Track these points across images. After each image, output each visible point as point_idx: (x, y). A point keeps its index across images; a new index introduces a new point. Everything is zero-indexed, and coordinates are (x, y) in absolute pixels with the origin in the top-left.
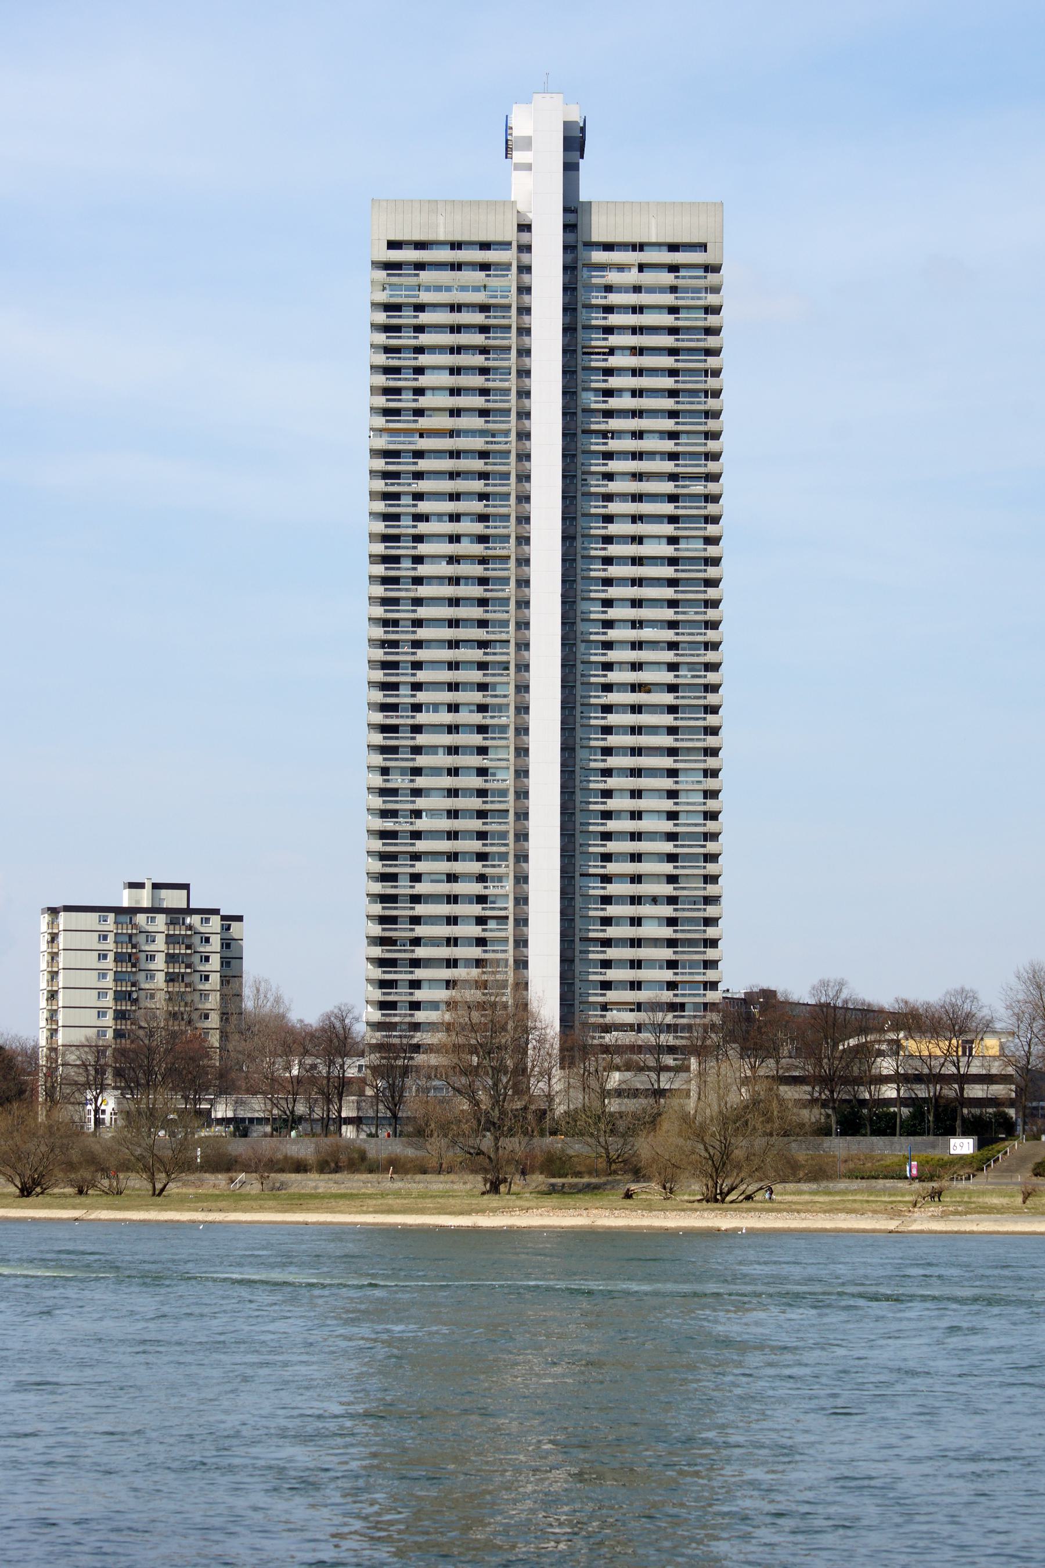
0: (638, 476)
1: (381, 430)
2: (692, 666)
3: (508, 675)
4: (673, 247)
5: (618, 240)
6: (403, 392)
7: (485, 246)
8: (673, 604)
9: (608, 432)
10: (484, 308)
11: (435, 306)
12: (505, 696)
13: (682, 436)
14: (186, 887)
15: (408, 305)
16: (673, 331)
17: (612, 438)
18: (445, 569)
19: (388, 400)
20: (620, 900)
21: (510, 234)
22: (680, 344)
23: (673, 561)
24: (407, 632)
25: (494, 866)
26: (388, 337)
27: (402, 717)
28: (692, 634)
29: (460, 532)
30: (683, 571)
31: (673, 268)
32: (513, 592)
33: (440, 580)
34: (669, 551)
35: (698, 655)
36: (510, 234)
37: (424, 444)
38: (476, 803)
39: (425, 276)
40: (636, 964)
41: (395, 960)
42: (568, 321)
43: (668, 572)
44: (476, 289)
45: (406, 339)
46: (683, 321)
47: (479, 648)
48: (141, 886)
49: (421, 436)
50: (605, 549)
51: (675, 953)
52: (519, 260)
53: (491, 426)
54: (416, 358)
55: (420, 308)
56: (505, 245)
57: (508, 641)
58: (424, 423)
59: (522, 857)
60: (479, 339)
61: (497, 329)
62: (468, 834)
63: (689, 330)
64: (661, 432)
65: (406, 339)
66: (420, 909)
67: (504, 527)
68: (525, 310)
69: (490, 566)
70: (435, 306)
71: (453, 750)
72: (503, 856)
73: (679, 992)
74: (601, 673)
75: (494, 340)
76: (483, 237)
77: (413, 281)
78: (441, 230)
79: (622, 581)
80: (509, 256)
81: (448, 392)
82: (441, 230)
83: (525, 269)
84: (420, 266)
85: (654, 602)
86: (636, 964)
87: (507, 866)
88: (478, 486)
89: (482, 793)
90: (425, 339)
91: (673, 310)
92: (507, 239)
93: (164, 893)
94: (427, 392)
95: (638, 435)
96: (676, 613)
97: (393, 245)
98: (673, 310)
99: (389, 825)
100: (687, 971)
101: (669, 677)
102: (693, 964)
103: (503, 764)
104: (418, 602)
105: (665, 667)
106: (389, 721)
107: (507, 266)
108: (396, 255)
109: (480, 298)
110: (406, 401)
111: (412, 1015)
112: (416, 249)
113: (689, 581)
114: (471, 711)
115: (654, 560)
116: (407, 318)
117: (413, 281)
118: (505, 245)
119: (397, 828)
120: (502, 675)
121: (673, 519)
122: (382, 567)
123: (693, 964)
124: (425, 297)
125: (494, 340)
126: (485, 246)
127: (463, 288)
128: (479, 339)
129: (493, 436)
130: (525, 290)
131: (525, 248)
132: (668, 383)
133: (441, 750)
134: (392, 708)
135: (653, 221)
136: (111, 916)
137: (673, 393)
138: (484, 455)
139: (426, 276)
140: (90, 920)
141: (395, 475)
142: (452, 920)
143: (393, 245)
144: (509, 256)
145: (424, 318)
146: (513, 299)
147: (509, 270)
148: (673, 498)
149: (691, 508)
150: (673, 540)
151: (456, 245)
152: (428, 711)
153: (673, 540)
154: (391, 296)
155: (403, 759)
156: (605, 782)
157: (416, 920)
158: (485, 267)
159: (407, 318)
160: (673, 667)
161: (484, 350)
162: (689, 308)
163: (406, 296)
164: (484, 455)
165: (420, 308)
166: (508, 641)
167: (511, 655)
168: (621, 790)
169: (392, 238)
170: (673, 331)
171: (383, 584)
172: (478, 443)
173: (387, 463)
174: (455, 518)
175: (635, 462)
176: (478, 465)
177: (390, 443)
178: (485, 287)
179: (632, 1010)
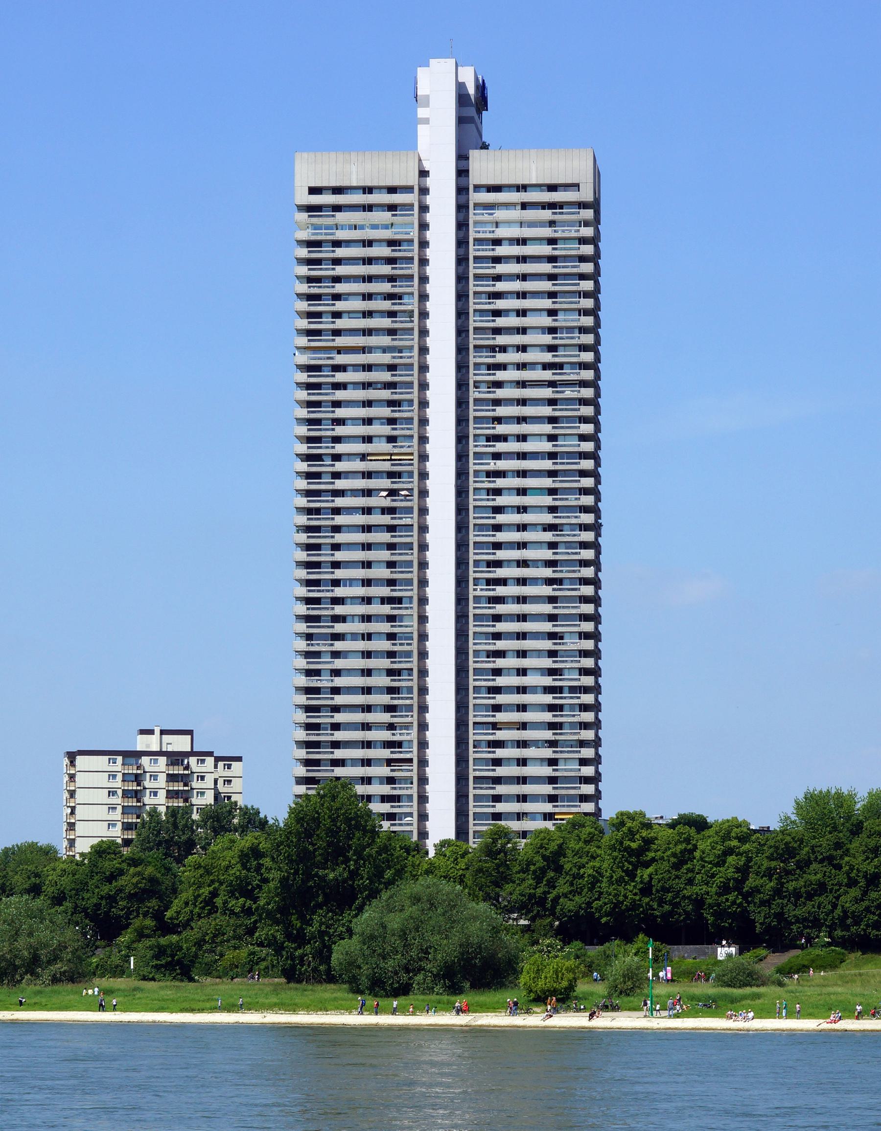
0: (522, 384)
1: (305, 348)
2: (569, 545)
3: (412, 554)
4: (552, 188)
5: (503, 183)
6: (324, 315)
7: (392, 190)
8: (552, 600)
9: (497, 346)
10: (391, 243)
11: (348, 243)
12: (411, 357)
13: (560, 313)
14: (190, 732)
15: (327, 241)
16: (552, 259)
17: (500, 352)
18: (361, 591)
19: (309, 394)
20: (509, 690)
21: (413, 179)
22: (556, 271)
23: (552, 456)
24: (327, 609)
25: (402, 716)
26: (309, 305)
27: (323, 591)
28: (568, 517)
29: (371, 362)
30: (561, 499)
31: (552, 206)
32: (417, 234)
33: (355, 492)
34: (547, 771)
35: (575, 535)
36: (413, 179)
37: (340, 359)
38: (386, 699)
39: (340, 217)
40: (523, 744)
41: (319, 724)
42: (459, 341)
43: (548, 789)
44: (386, 227)
45: (325, 271)
46: (560, 251)
47: (388, 406)
48: (151, 732)
49: (339, 353)
50: (494, 410)
51: (554, 788)
52: (420, 202)
53: (396, 343)
54: (333, 287)
55: (337, 244)
56: (408, 189)
57: (412, 525)
58: (340, 341)
59: (423, 708)
60: (386, 270)
61: (403, 263)
62: (379, 618)
63: (566, 258)
64: (542, 760)
65: (325, 271)
66: (339, 574)
67: (408, 429)
68: (424, 244)
69: (398, 284)
70: (348, 243)
71: (367, 618)
72: (409, 510)
73: (558, 461)
74: (491, 408)
75: (400, 270)
76: (390, 183)
77: (329, 221)
78: (354, 177)
79: (509, 527)
80: (411, 198)
81: (361, 297)
82: (354, 177)
83: (424, 209)
84: (337, 208)
85: (536, 599)
86: (523, 744)
87: (412, 716)
88: (386, 394)
89: (391, 637)
90: (339, 700)
91: (552, 241)
92: (410, 184)
93: (166, 738)
94: (344, 315)
95: (522, 438)
96: (554, 410)
97: (313, 191)
98: (552, 241)
99: (314, 682)
100: (566, 804)
101: (548, 554)
102: (571, 798)
103: (408, 612)
104: (336, 547)
105: (546, 545)
106: (312, 595)
107: (410, 206)
108: (316, 200)
109: (387, 234)
110: (326, 324)
111: (333, 555)
112: (333, 193)
113: (566, 473)
114: (382, 424)
115: (535, 456)
116: (325, 253)
117: (329, 221)
118: (408, 189)
119: (319, 684)
120: (407, 554)
121: (552, 420)
122: (306, 321)
123: (571, 798)
124: (341, 235)
125: (400, 270)
126: (392, 190)
127: (374, 227)
128: (386, 270)
129: (400, 351)
130: (424, 226)
131: (424, 191)
132: (548, 609)
133: (356, 619)
134: (316, 583)
135: (534, 167)
136: (120, 759)
137: (552, 277)
138: (392, 368)
139: (341, 217)
140: (101, 762)
141: (318, 440)
142: (368, 565)
143: (313, 191)
144: (411, 198)
145: (340, 252)
146: (414, 234)
147: (412, 424)
148: (552, 402)
149: (566, 410)
150: (552, 438)
151: (368, 190)
152: (345, 586)
153: (552, 438)
154: (314, 234)
155: (324, 305)
156: (495, 644)
157: (337, 457)
158: (392, 208)
159: (325, 253)
160: (552, 545)
161: (391, 279)
162: (565, 239)
163: (326, 234)
164: (392, 368)
165: (337, 244)
166: (412, 525)
167: (412, 520)
168: (509, 489)
169: (313, 185)
170: (552, 259)
171: (307, 389)
172: (387, 358)
173: (309, 376)
174: (368, 421)
175: (519, 749)
176: (386, 376)
177: (314, 234)
178: (392, 224)
179: (518, 729)
